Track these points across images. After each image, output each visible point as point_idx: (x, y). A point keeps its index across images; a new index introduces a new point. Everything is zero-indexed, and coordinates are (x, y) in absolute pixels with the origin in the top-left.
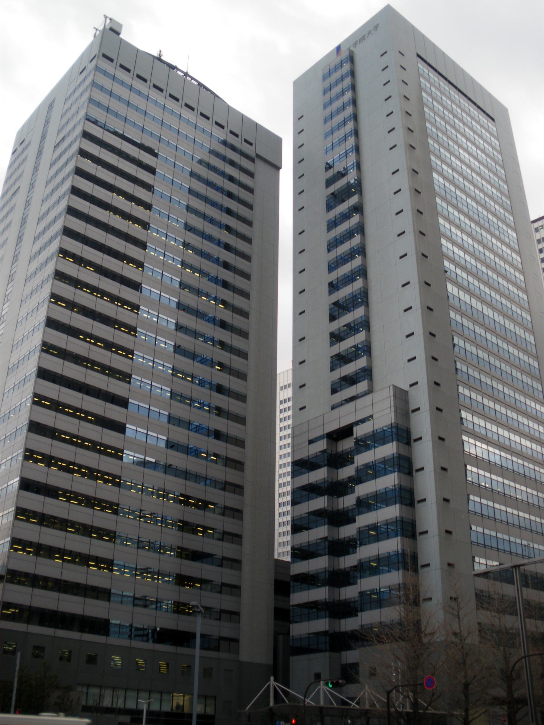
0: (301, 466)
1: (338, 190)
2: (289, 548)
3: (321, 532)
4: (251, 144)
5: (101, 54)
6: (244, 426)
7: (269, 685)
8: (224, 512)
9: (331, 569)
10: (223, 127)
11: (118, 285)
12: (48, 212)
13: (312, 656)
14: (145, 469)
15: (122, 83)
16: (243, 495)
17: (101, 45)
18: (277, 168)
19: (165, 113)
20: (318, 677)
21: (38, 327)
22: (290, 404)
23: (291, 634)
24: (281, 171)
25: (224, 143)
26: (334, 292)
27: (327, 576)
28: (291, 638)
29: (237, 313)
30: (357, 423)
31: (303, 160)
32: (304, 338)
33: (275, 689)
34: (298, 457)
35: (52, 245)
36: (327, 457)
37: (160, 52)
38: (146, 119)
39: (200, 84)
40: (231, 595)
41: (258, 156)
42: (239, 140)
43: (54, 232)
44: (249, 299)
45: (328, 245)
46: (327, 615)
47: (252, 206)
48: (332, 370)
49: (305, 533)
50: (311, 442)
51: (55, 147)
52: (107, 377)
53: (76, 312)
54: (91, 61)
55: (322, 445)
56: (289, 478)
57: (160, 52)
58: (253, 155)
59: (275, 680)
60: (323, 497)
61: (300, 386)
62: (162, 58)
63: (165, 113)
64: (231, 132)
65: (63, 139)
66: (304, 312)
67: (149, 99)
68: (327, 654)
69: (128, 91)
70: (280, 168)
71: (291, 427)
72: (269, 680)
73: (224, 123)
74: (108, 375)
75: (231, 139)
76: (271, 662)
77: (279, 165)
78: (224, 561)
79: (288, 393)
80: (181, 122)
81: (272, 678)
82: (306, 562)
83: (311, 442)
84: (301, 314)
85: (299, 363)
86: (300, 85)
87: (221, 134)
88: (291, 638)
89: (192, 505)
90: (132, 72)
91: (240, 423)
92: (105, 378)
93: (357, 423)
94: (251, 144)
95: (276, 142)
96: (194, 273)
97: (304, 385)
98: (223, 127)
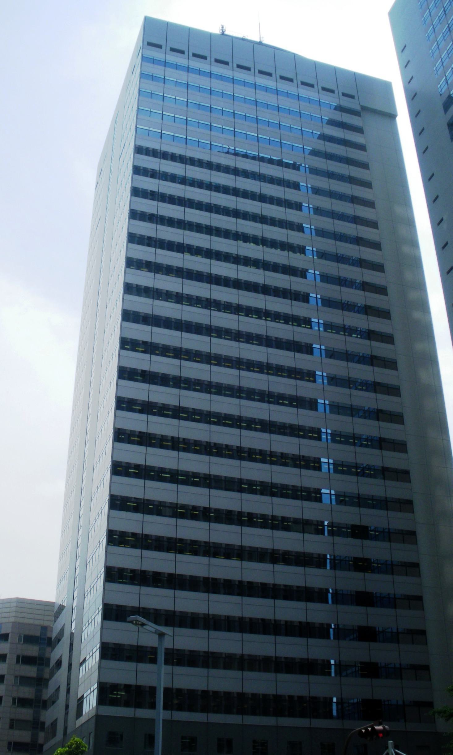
4: (352, 97)
14: (392, 544)
17: (144, 34)
18: (392, 116)
25: (340, 109)
30: (153, 633)
31: (416, 94)
37: (223, 27)
41: (363, 108)
42: (336, 95)
52: (296, 409)
53: (347, 335)
57: (223, 27)
58: (358, 108)
62: (226, 33)
63: (322, 108)
64: (344, 95)
67: (321, 103)
69: (209, 79)
74: (296, 407)
75: (346, 103)
77: (393, 113)
87: (332, 100)
90: (274, 75)
92: (294, 410)
93: (153, 633)
94: (352, 97)
95: (386, 87)
98: (332, 91)
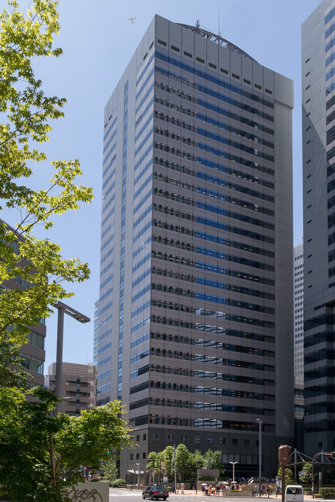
0: (309, 324)
2: (303, 357)
3: (322, 345)
5: (157, 41)
6: (273, 163)
7: (294, 453)
8: (264, 398)
9: (328, 367)
12: (140, 162)
13: (317, 433)
16: (275, 371)
17: (155, 32)
20: (320, 445)
21: (147, 273)
22: (302, 269)
23: (305, 421)
26: (331, 174)
27: (325, 371)
28: (305, 423)
29: (267, 145)
32: (311, 240)
33: (297, 455)
34: (307, 336)
35: (148, 185)
36: (326, 353)
39: (230, 44)
40: (270, 328)
43: (148, 146)
44: (274, 148)
45: (329, 239)
46: (326, 411)
47: (273, 118)
48: (328, 191)
49: (312, 347)
50: (316, 308)
51: (136, 123)
54: (151, 47)
55: (322, 311)
56: (302, 331)
57: (198, 22)
59: (297, 450)
60: (323, 325)
61: (308, 256)
65: (141, 118)
66: (311, 221)
67: (194, 143)
68: (326, 432)
70: (293, 108)
71: (303, 334)
72: (294, 450)
76: (294, 436)
78: (265, 411)
79: (301, 262)
81: (295, 449)
82: (313, 364)
83: (316, 308)
84: (309, 222)
85: (308, 240)
86: (307, 28)
88: (305, 423)
89: (245, 322)
91: (270, 160)
96: (237, 176)
97: (311, 271)
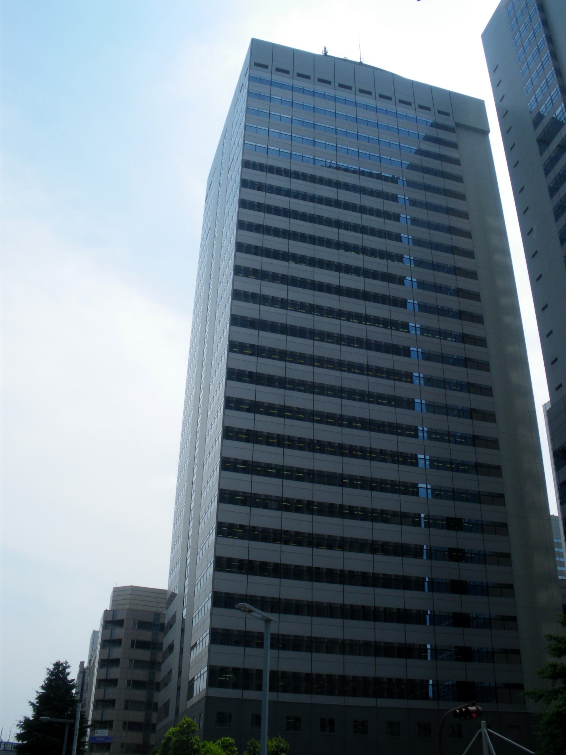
1: (546, 126)
10: (428, 109)
11: (311, 292)
15: (303, 91)
18: (485, 132)
19: (358, 109)
24: (490, 135)
25: (435, 125)
30: (259, 619)
37: (325, 49)
38: (316, 114)
41: (458, 125)
57: (325, 49)
58: (452, 124)
62: (328, 54)
64: (439, 112)
69: (333, 103)
73: (429, 105)
74: (395, 406)
75: (441, 119)
80: (316, 98)
92: (392, 409)
93: (259, 619)
